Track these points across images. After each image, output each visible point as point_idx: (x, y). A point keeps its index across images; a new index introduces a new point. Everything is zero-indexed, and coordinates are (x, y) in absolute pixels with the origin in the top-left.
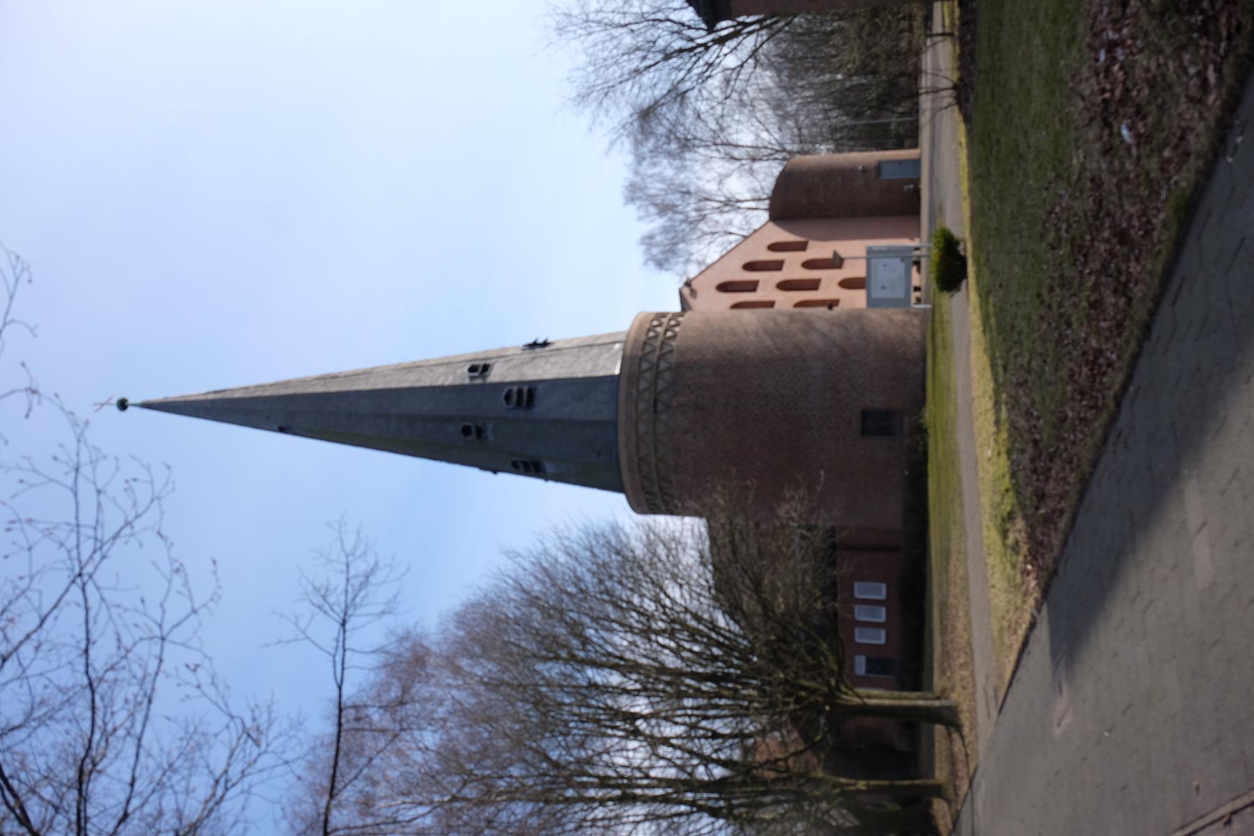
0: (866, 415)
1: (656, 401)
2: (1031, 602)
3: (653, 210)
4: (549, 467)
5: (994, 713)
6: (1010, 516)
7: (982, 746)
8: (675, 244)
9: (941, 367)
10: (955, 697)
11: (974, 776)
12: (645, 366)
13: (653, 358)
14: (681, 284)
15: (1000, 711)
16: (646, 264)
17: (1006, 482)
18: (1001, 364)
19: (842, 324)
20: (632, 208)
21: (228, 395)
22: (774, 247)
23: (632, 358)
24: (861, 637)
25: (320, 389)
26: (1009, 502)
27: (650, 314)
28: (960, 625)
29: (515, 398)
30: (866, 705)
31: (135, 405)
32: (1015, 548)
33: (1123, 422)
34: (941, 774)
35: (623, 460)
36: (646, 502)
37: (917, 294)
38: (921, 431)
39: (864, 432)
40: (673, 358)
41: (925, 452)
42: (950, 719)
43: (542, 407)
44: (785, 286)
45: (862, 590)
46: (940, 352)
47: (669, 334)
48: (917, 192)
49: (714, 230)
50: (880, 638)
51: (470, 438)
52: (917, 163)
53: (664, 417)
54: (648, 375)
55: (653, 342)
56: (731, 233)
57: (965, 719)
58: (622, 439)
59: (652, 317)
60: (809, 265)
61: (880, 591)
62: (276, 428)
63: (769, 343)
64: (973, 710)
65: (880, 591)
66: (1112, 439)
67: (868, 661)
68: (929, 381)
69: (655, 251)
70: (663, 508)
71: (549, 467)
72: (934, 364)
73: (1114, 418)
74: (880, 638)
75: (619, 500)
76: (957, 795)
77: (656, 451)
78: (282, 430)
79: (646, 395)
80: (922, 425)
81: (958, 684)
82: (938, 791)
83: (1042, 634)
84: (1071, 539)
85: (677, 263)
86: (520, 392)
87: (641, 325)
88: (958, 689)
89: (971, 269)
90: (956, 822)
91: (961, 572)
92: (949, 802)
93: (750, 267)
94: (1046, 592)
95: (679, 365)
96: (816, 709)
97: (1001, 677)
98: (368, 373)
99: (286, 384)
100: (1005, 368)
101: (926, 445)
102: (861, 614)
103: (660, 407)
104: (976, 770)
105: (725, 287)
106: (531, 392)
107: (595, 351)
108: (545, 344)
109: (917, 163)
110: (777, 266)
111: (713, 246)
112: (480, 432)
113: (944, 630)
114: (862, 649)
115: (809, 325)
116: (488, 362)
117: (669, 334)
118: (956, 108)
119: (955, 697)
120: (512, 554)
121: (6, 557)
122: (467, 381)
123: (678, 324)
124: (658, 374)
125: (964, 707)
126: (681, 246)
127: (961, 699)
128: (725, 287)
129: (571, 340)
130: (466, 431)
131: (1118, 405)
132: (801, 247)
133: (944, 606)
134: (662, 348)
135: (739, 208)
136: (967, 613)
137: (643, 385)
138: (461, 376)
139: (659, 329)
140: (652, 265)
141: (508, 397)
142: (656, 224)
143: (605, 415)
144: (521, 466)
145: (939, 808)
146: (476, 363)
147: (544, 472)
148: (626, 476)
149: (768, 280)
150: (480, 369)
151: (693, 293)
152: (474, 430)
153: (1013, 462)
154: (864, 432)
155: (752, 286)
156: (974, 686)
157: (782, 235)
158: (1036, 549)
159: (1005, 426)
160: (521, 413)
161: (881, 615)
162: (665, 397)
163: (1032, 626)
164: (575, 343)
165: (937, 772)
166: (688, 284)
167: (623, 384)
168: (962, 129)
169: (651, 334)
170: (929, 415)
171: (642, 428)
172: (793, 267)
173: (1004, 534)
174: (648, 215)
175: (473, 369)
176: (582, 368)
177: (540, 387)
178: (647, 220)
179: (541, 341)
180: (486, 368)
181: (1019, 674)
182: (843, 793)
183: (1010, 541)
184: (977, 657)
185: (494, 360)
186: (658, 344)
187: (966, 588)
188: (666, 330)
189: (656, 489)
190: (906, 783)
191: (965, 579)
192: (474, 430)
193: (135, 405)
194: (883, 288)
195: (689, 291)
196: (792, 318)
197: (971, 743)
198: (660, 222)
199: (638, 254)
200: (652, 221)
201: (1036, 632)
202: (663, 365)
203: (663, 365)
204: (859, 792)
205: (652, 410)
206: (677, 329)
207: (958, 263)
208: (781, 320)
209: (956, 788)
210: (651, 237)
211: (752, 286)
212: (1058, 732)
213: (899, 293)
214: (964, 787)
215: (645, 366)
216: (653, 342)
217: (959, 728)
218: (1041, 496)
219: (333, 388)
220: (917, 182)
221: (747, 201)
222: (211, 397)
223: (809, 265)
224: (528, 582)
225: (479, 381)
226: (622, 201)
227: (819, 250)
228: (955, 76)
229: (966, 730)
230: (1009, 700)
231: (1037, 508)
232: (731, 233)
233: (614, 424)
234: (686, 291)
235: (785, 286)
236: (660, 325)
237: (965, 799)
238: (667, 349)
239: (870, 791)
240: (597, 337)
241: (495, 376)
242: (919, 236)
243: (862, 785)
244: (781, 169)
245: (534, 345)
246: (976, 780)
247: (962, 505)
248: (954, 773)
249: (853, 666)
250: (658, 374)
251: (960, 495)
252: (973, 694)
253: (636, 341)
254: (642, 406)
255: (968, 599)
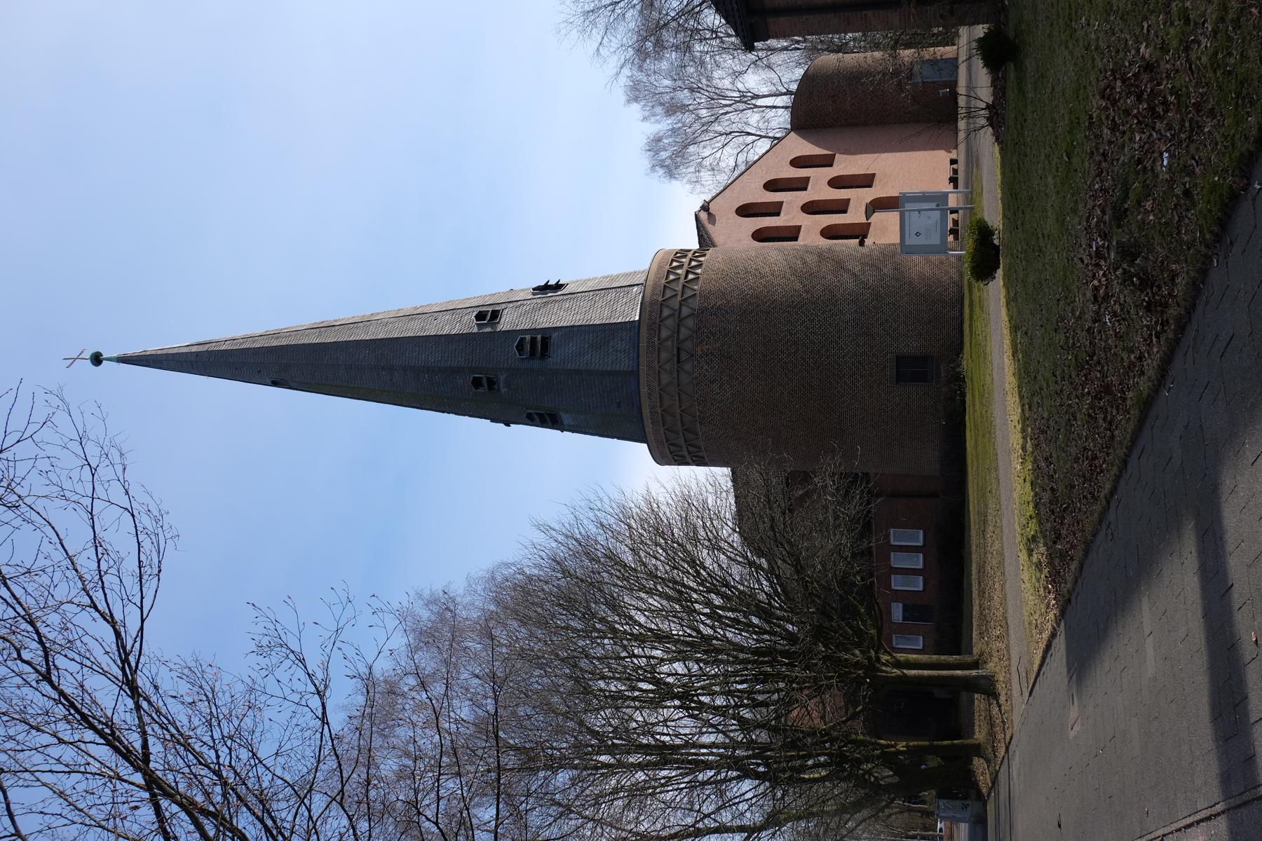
0: (901, 360)
2: (1051, 616)
3: (659, 110)
4: (566, 418)
7: (1016, 718)
8: (686, 147)
9: (978, 325)
11: (1010, 743)
12: (666, 312)
13: (675, 303)
14: (698, 208)
17: (1030, 510)
20: (636, 107)
22: (797, 162)
23: (652, 303)
24: (897, 583)
25: (315, 340)
26: (1033, 528)
27: (669, 252)
30: (905, 675)
32: (1039, 566)
33: (1111, 516)
34: (980, 735)
35: (646, 411)
36: (668, 453)
37: (955, 216)
38: (958, 381)
39: (900, 378)
40: (695, 304)
42: (988, 688)
43: (559, 356)
44: (811, 208)
46: (977, 309)
47: (691, 276)
48: (954, 95)
50: (918, 584)
51: (481, 390)
52: (953, 63)
53: (688, 367)
54: (669, 322)
55: (673, 286)
57: (1000, 687)
58: (644, 390)
59: (672, 257)
60: (836, 183)
61: (918, 538)
62: (270, 383)
64: (1008, 682)
65: (918, 538)
67: (905, 609)
69: (664, 155)
70: (690, 461)
71: (566, 418)
72: (971, 326)
73: (1106, 510)
74: (918, 584)
75: (639, 452)
76: (996, 756)
78: (275, 384)
80: (959, 373)
81: (995, 654)
82: (977, 750)
83: (1060, 644)
86: (533, 340)
87: (660, 267)
89: (1001, 266)
90: (995, 781)
91: (997, 546)
92: (988, 761)
93: (772, 186)
95: (703, 311)
96: (859, 682)
99: (276, 335)
101: (963, 395)
103: (684, 356)
104: (1011, 739)
105: (746, 211)
106: (546, 342)
107: (612, 295)
108: (558, 286)
110: (802, 185)
111: (727, 149)
112: (491, 383)
113: (982, 593)
114: (899, 596)
115: (839, 264)
116: (497, 308)
117: (691, 276)
119: (991, 666)
120: (545, 528)
122: (475, 330)
123: (700, 266)
124: (681, 321)
126: (692, 149)
128: (746, 211)
130: (477, 383)
131: (1108, 502)
132: (827, 162)
133: (981, 569)
135: (756, 106)
137: (665, 333)
138: (467, 324)
139: (679, 271)
140: (661, 171)
141: (520, 347)
143: (625, 365)
144: (536, 417)
145: (978, 764)
146: (484, 309)
147: (562, 423)
150: (488, 315)
151: (711, 217)
152: (485, 382)
153: (1036, 494)
154: (900, 378)
156: (1009, 659)
158: (1055, 577)
160: (536, 364)
161: (918, 562)
162: (688, 345)
163: (1053, 635)
165: (977, 735)
166: (705, 207)
167: (644, 331)
168: (997, 148)
170: (966, 363)
172: (819, 178)
175: (480, 316)
176: (598, 315)
177: (555, 335)
178: (653, 119)
179: (552, 282)
180: (495, 315)
181: (1044, 669)
182: (883, 753)
183: (1035, 559)
185: (503, 306)
186: (679, 288)
187: (1001, 563)
189: (681, 441)
192: (485, 382)
194: (918, 234)
195: (705, 218)
196: (821, 255)
198: (665, 125)
200: (658, 122)
201: (1056, 640)
202: (685, 311)
203: (685, 311)
205: (675, 359)
206: (699, 271)
209: (994, 750)
212: (1072, 734)
214: (1002, 751)
215: (666, 312)
216: (673, 286)
217: (996, 696)
219: (330, 338)
220: (953, 84)
223: (836, 183)
224: (562, 553)
225: (488, 330)
226: (623, 98)
227: (846, 165)
228: (990, 100)
229: (1002, 699)
230: (1037, 687)
231: (1055, 543)
233: (635, 374)
234: (703, 215)
235: (811, 208)
236: (680, 267)
238: (689, 293)
239: (910, 751)
240: (613, 278)
241: (507, 322)
243: (901, 746)
245: (545, 288)
246: (1012, 748)
247: (998, 479)
248: (992, 735)
249: (889, 613)
250: (681, 321)
251: (997, 469)
253: (655, 285)
254: (664, 355)
255: (1003, 574)
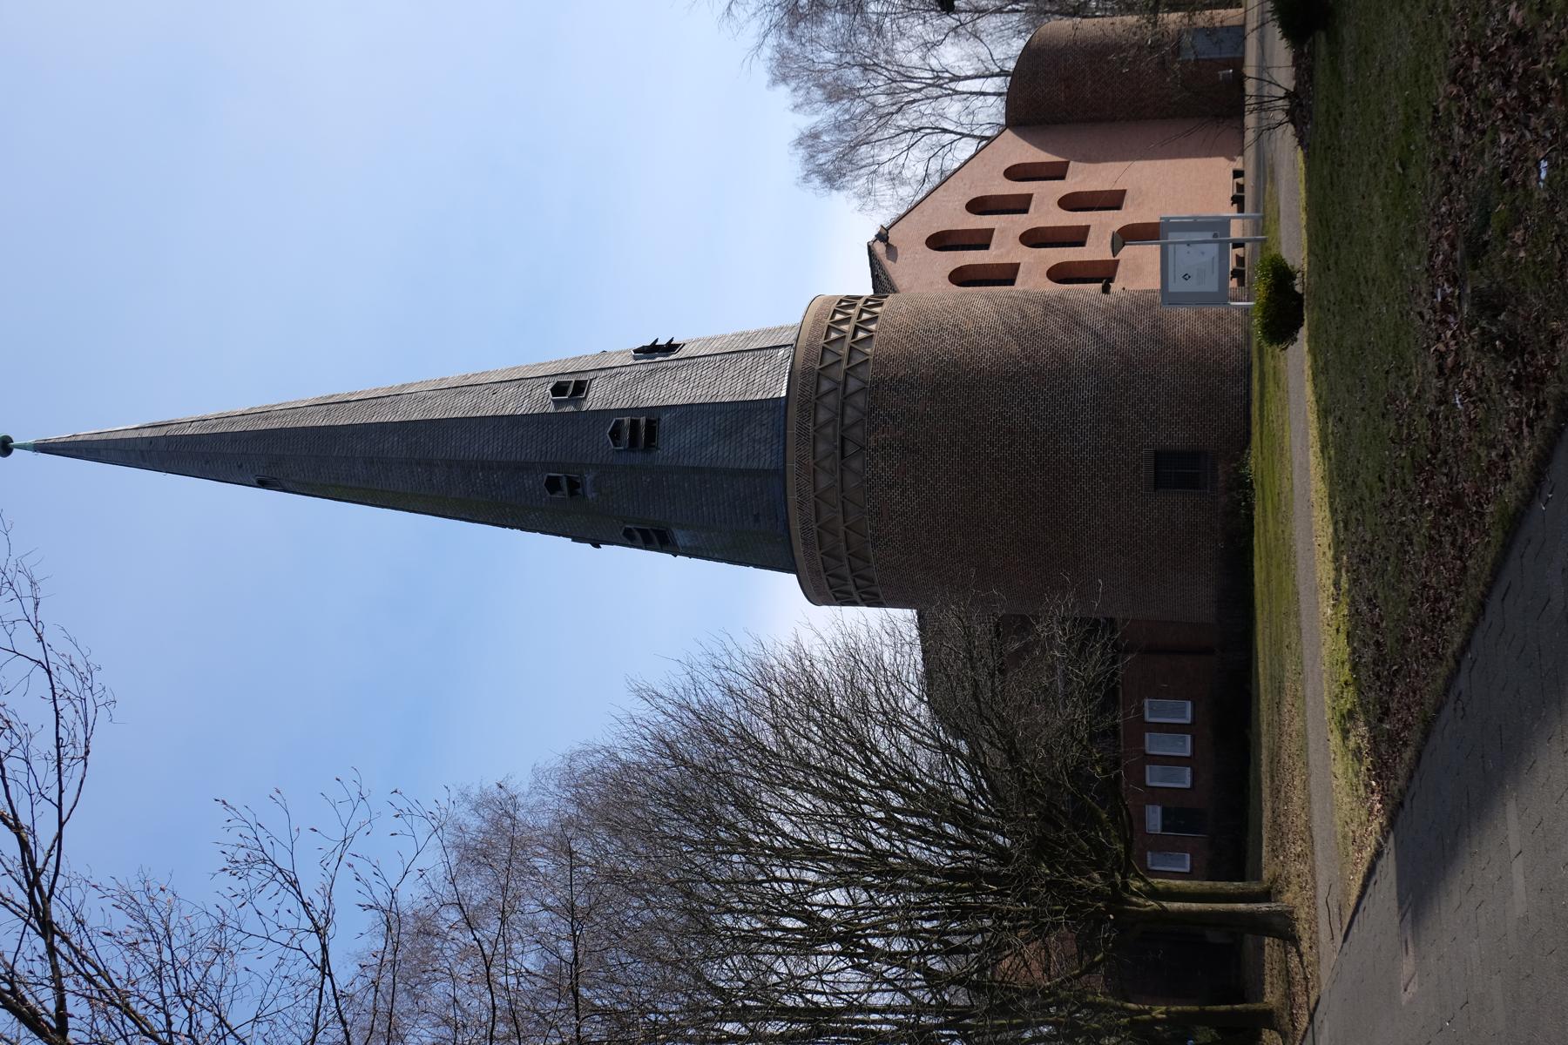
0: (1161, 458)
1: (843, 439)
2: (1375, 826)
3: (817, 94)
4: (681, 537)
5: (1339, 939)
6: (1350, 715)
7: (1325, 973)
9: (1272, 408)
10: (1290, 898)
11: (1315, 1009)
12: (826, 386)
13: (838, 373)
15: (1345, 939)
16: (806, 179)
17: (1346, 673)
18: (1346, 514)
19: (1121, 316)
20: (783, 90)
21: (173, 431)
22: (1015, 173)
24: (1155, 777)
26: (1349, 699)
27: (829, 300)
28: (1297, 797)
29: (627, 435)
31: (23, 447)
32: (1357, 753)
33: (1462, 683)
34: (1272, 997)
35: (796, 527)
38: (1243, 488)
39: (1159, 483)
40: (868, 374)
41: (1250, 518)
42: (1283, 929)
43: (670, 448)
44: (1034, 239)
45: (1154, 711)
46: (1271, 386)
48: (1240, 79)
49: (916, 124)
50: (1184, 779)
51: (558, 495)
53: (856, 464)
55: (835, 347)
56: (945, 131)
57: (1302, 928)
58: (792, 497)
60: (1071, 203)
61: (1185, 713)
63: (1014, 348)
64: (1313, 920)
65: (1185, 713)
66: (1465, 666)
67: (1166, 814)
68: (1255, 430)
70: (859, 600)
71: (681, 537)
72: (1261, 409)
76: (1295, 1028)
77: (845, 513)
78: (262, 484)
79: (829, 430)
80: (1245, 476)
81: (1294, 880)
82: (1268, 1019)
83: (1388, 865)
84: (1416, 776)
85: (856, 178)
86: (634, 424)
87: (817, 322)
88: (1295, 888)
89: (1306, 322)
91: (1297, 723)
94: (1391, 823)
97: (1347, 894)
98: (396, 396)
99: (265, 414)
100: (1346, 528)
101: (1250, 508)
102: (1155, 745)
103: (850, 449)
104: (1317, 1003)
105: (941, 242)
106: (652, 426)
107: (747, 360)
108: (671, 347)
109: (1239, 32)
110: (1020, 205)
111: (915, 152)
112: (574, 485)
113: (1276, 792)
114: (1156, 795)
115: (1073, 319)
118: (1291, 128)
119: (1290, 898)
120: (649, 695)
121: (289, 911)
122: (551, 409)
123: (873, 320)
124: (846, 398)
125: (1302, 913)
127: (1298, 902)
128: (941, 242)
129: (710, 340)
130: (553, 485)
131: (1458, 663)
132: (1056, 172)
133: (1275, 758)
134: (850, 358)
135: (956, 92)
136: (1306, 783)
137: (823, 416)
138: (540, 401)
139: (845, 327)
140: (817, 181)
141: (616, 434)
142: (823, 115)
144: (638, 535)
147: (675, 544)
148: (799, 552)
149: (1006, 227)
150: (570, 388)
151: (891, 251)
152: (564, 483)
153: (1354, 651)
154: (1159, 483)
155: (982, 240)
156: (1315, 888)
157: (1029, 153)
158: (1381, 770)
159: (1345, 600)
160: (638, 458)
161: (1183, 746)
162: (857, 432)
163: (1378, 854)
164: (716, 347)
166: (882, 237)
167: (793, 411)
168: (1300, 154)
169: (834, 335)
170: (1255, 461)
171: (824, 481)
173: (1345, 734)
174: (809, 101)
175: (559, 389)
176: (728, 388)
177: (665, 417)
179: (663, 342)
180: (580, 387)
181: (1364, 902)
182: (1133, 1023)
183: (1352, 744)
184: (1318, 848)
186: (844, 351)
187: (1303, 749)
188: (856, 329)
189: (846, 571)
190: (1223, 1008)
191: (1303, 735)
192: (564, 483)
193: (23, 447)
194: (1186, 277)
197: (1310, 964)
199: (791, 163)
200: (817, 113)
201: (1382, 862)
202: (853, 384)
203: (853, 384)
204: (1156, 1021)
205: (838, 452)
206: (873, 327)
207: (1295, 303)
208: (1034, 311)
210: (815, 136)
211: (982, 240)
212: (1405, 998)
213: (1211, 285)
214: (1304, 1021)
215: (826, 386)
217: (1295, 941)
218: (1386, 712)
220: (1238, 63)
221: (967, 78)
222: (146, 433)
223: (1071, 203)
224: (673, 731)
227: (1085, 177)
229: (1305, 946)
232: (945, 131)
233: (780, 473)
234: (880, 248)
235: (1034, 239)
236: (846, 321)
237: (1304, 1037)
238: (859, 358)
239: (1171, 1019)
240: (749, 337)
241: (596, 399)
242: (1242, 153)
243: (1159, 1012)
244: (1018, 45)
245: (652, 350)
248: (1289, 996)
250: (846, 398)
251: (1297, 614)
252: (1314, 906)
255: (1306, 764)
